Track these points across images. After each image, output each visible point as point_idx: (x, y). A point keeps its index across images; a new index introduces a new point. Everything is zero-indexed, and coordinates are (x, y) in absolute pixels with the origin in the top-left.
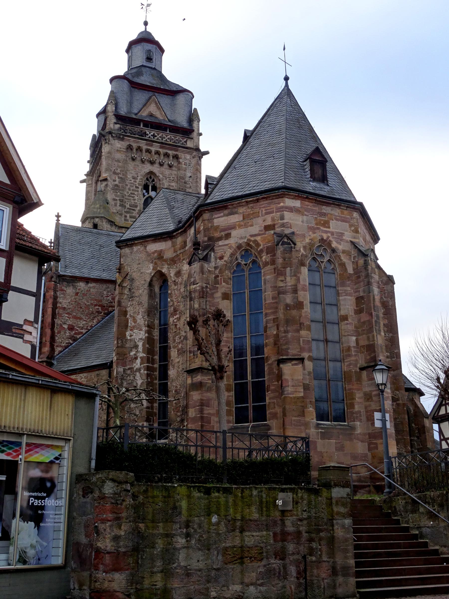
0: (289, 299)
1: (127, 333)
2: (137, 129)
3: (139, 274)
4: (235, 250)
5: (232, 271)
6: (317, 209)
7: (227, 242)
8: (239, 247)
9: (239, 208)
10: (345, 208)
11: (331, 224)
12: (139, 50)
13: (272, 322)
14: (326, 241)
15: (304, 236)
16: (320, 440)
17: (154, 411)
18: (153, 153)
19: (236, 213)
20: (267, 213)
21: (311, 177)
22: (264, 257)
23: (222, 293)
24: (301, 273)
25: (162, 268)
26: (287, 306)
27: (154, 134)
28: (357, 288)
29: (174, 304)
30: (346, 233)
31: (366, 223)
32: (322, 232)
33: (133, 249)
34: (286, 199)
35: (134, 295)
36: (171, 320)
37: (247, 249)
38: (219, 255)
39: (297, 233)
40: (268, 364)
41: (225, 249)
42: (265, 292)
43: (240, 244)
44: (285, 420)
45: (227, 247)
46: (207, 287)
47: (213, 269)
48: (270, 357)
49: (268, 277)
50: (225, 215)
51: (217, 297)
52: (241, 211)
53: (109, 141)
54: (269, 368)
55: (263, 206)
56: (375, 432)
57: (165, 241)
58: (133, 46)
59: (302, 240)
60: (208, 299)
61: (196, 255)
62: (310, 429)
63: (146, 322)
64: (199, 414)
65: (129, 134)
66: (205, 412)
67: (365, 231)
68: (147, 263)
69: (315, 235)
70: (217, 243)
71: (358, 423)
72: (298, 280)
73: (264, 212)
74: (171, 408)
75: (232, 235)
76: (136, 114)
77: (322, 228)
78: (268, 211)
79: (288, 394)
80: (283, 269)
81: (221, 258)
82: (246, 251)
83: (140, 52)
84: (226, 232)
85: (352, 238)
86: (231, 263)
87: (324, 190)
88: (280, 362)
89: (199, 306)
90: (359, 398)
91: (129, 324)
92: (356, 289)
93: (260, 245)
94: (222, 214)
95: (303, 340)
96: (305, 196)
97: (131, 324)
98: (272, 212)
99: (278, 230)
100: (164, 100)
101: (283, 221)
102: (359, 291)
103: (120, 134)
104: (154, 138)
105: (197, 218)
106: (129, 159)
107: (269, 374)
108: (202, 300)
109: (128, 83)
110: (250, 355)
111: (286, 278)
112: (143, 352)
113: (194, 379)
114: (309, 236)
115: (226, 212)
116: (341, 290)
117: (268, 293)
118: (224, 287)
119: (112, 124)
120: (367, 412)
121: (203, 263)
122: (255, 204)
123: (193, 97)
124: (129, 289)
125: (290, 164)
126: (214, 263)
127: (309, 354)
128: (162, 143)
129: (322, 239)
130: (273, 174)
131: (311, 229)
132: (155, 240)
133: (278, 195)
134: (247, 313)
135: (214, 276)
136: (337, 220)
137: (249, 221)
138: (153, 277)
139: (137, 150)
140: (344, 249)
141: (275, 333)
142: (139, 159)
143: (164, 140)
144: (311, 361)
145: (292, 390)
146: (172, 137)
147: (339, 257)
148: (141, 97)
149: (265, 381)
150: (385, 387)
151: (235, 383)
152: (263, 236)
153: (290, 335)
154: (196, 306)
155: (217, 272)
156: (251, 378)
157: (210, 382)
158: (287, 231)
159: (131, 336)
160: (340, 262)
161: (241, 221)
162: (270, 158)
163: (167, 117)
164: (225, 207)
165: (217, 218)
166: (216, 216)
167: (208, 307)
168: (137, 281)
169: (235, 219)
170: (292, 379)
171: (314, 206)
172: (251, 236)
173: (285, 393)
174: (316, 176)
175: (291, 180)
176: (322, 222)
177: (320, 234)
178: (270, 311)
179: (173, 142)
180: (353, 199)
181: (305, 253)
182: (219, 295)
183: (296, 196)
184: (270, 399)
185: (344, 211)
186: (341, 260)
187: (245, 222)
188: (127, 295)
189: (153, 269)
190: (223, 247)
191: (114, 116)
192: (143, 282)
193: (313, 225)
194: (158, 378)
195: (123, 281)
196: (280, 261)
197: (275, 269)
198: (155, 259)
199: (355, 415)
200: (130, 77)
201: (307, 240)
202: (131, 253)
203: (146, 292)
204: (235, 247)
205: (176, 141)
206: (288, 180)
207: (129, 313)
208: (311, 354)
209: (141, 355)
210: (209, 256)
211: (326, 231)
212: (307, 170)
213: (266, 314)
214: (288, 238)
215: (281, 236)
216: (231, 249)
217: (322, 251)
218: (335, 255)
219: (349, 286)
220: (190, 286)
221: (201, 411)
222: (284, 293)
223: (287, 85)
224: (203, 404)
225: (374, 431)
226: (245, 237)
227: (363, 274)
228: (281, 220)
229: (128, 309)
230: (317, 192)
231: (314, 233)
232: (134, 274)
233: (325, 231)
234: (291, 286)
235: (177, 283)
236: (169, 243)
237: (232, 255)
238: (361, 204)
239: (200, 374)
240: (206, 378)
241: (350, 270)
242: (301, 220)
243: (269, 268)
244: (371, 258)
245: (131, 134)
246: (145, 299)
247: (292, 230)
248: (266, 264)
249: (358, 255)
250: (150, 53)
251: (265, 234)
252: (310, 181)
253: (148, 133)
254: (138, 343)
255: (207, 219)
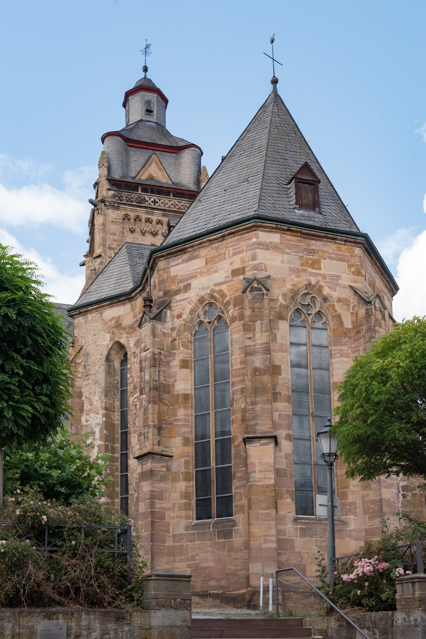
0: (258, 361)
1: (83, 419)
2: (134, 196)
3: (95, 347)
4: (196, 304)
5: (193, 333)
6: (303, 244)
7: (186, 295)
8: (201, 300)
9: (201, 250)
10: (343, 243)
11: (322, 264)
12: (137, 103)
13: (240, 393)
14: (314, 286)
15: (284, 280)
16: (299, 538)
17: (116, 507)
18: (154, 222)
19: (197, 257)
20: (235, 254)
21: (296, 203)
22: (231, 311)
23: (180, 361)
24: (278, 329)
25: (120, 338)
26: (256, 370)
27: (155, 200)
28: (356, 347)
29: (133, 380)
30: (343, 275)
31: (375, 264)
32: (310, 275)
33: (87, 317)
34: (260, 233)
35: (89, 373)
36: (131, 399)
37: (209, 302)
38: (176, 313)
39: (275, 276)
40: (235, 446)
41: (183, 305)
42: (232, 355)
43: (202, 297)
44: (250, 514)
45: (186, 302)
46: (160, 353)
47: (170, 331)
48: (236, 437)
49: (235, 336)
50: (183, 262)
51: (173, 367)
52: (203, 255)
53: (102, 211)
54: (235, 450)
55: (230, 245)
56: (374, 528)
57: (124, 304)
58: (130, 98)
59: (280, 286)
60: (162, 368)
61: (147, 315)
62: (286, 525)
63: (104, 404)
64: (149, 509)
65: (125, 202)
66: (157, 506)
67: (374, 274)
68: (103, 333)
69: (299, 279)
70: (174, 298)
71: (352, 517)
72: (274, 338)
73: (231, 252)
74: (131, 503)
75: (192, 286)
76: (134, 178)
77: (310, 270)
78: (236, 250)
79: (255, 481)
80: (251, 323)
81: (179, 316)
82: (210, 304)
83: (137, 103)
84: (185, 283)
85: (351, 282)
86: (191, 321)
87: (315, 219)
88: (246, 441)
89: (150, 378)
90: (354, 486)
91: (85, 408)
92: (354, 348)
93: (226, 296)
94: (180, 261)
95: (280, 415)
96: (285, 228)
97: (87, 407)
98: (241, 252)
99: (249, 274)
100: (168, 159)
101: (256, 262)
102: (359, 350)
103: (115, 202)
104: (155, 205)
105: (152, 269)
106: (127, 231)
107: (235, 458)
108: (153, 369)
109: (123, 141)
110: (214, 436)
111: (254, 335)
112: (101, 439)
113: (144, 467)
114: (292, 280)
115: (185, 256)
116: (334, 350)
117: (236, 356)
118: (182, 353)
119: (107, 192)
120: (364, 503)
121: (155, 323)
122: (220, 243)
123: (202, 154)
124: (85, 365)
125: (268, 188)
126: (170, 323)
127: (287, 432)
128: (165, 210)
129: (310, 284)
130: (245, 203)
131: (293, 271)
132: (112, 303)
133: (249, 228)
134: (210, 384)
135: (170, 339)
136: (331, 258)
137: (212, 266)
138: (111, 349)
139: (135, 220)
140: (339, 296)
141: (243, 406)
142: (138, 230)
143: (167, 206)
144: (290, 441)
145: (261, 476)
146: (177, 203)
147: (333, 307)
148: (138, 157)
149: (231, 466)
150: (335, 458)
151: (196, 471)
152: (230, 283)
153: (258, 407)
154: (147, 377)
155: (174, 334)
156: (214, 464)
157: (165, 469)
158: (261, 275)
159: (87, 421)
160: (334, 314)
161: (203, 267)
162: (244, 183)
163: (170, 180)
164: (183, 251)
165: (174, 266)
166: (173, 264)
167: (162, 378)
168: (92, 356)
169: (197, 264)
170: (260, 463)
171: (299, 241)
172: (216, 285)
173: (251, 480)
174: (304, 202)
175: (269, 208)
176: (310, 262)
177: (307, 278)
178: (237, 379)
179: (177, 209)
180: (354, 230)
181: (284, 303)
182: (176, 363)
183: (273, 228)
184: (236, 488)
185: (341, 246)
186: (336, 311)
187: (208, 268)
188: (82, 373)
189: (110, 340)
190: (181, 303)
191: (106, 182)
192: (99, 357)
193: (297, 265)
194: (119, 469)
195: (76, 356)
196: (248, 312)
197: (244, 325)
198: (113, 328)
199: (347, 507)
200: (125, 134)
201: (289, 286)
202: (86, 322)
203: (103, 368)
204: (195, 301)
205: (181, 207)
206: (263, 207)
207: (84, 395)
208: (291, 432)
209: (98, 442)
210: (163, 315)
211: (315, 273)
212: (292, 194)
213: (233, 383)
214: (259, 283)
215: (249, 282)
216: (190, 304)
217: (309, 301)
218: (326, 304)
219: (345, 345)
220: (140, 353)
221: (152, 505)
222: (252, 354)
223: (275, 91)
224: (153, 497)
225: (371, 527)
226: (208, 287)
227: (364, 328)
228: (252, 260)
229: (83, 390)
230: (306, 222)
231: (299, 276)
232: (89, 347)
233: (313, 273)
234: (261, 344)
235: (137, 354)
236: (128, 306)
237: (192, 312)
238: (366, 237)
239: (150, 460)
240: (158, 465)
241: (348, 323)
242: (280, 259)
243: (238, 324)
244: (375, 307)
245: (127, 201)
246: (101, 376)
247: (267, 273)
248: (233, 319)
249: (359, 303)
250: (150, 104)
251: (233, 281)
252: (295, 208)
253: (147, 199)
254: (95, 429)
255: (163, 268)
